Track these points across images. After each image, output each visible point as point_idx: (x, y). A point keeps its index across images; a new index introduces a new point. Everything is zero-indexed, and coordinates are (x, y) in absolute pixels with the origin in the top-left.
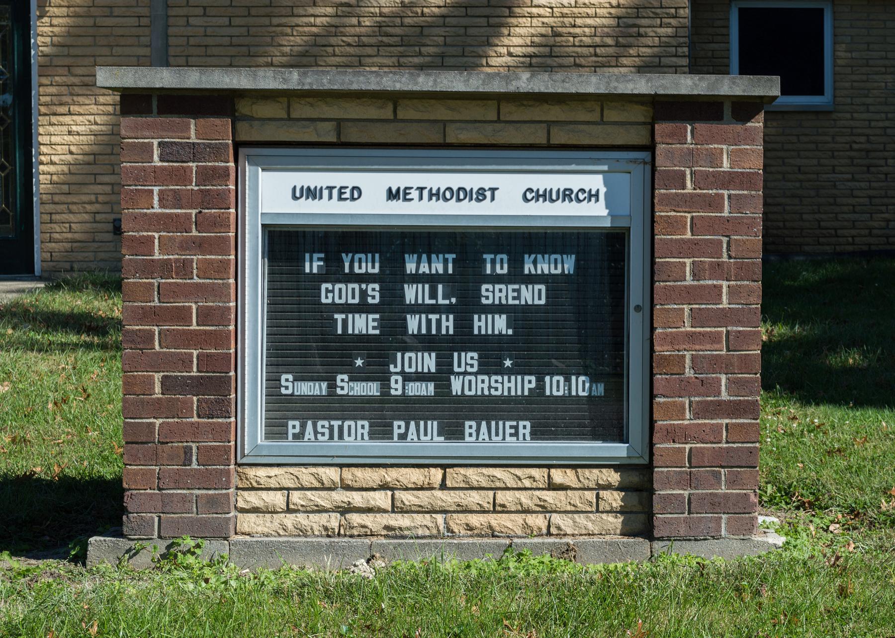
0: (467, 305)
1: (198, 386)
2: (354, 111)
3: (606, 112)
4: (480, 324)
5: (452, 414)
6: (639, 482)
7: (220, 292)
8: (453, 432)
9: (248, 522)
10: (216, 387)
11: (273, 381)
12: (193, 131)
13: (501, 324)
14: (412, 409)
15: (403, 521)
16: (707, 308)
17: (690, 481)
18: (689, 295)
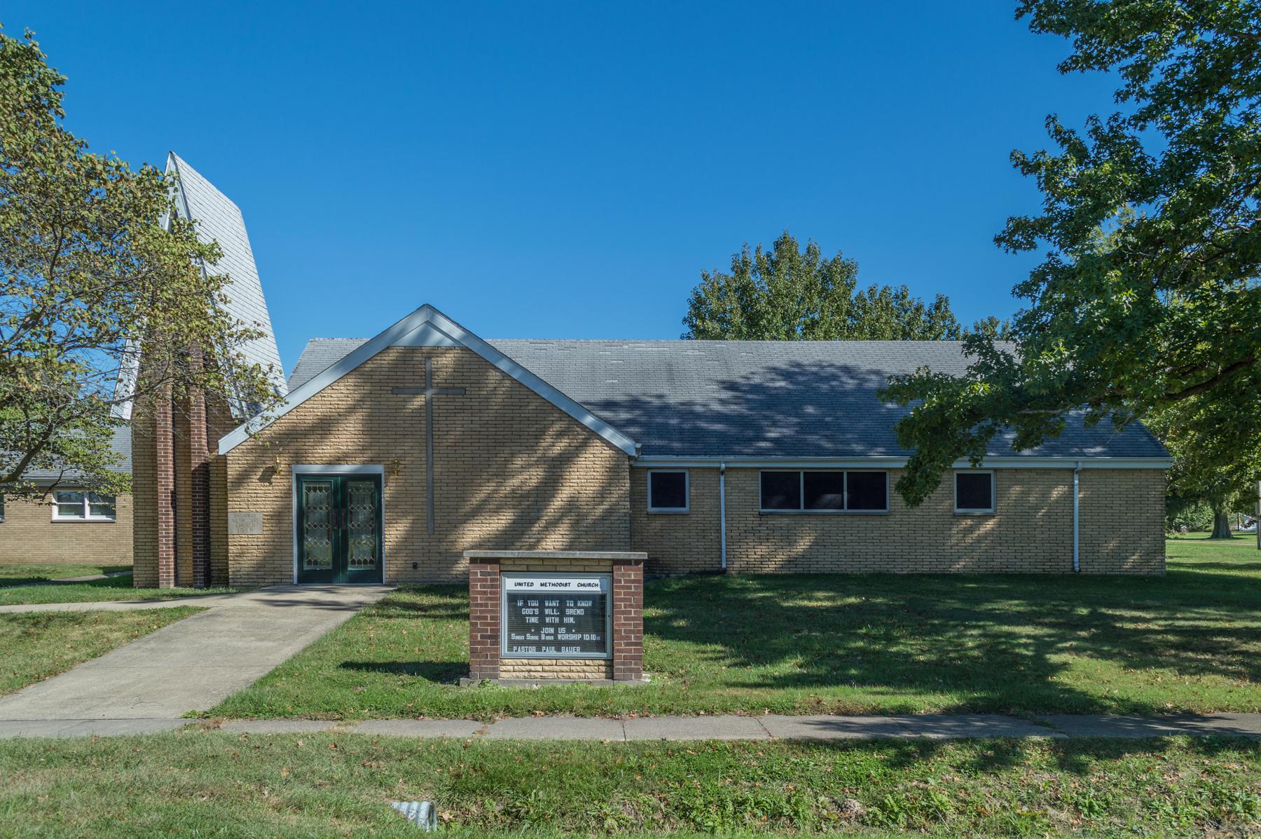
0: (562, 614)
1: (490, 637)
2: (532, 562)
3: (608, 452)
4: (566, 620)
5: (558, 645)
6: (610, 664)
7: (495, 612)
8: (559, 650)
9: (503, 674)
10: (495, 638)
11: (509, 636)
12: (489, 568)
13: (571, 620)
14: (547, 643)
15: (545, 674)
16: (630, 611)
17: (624, 664)
18: (623, 613)
